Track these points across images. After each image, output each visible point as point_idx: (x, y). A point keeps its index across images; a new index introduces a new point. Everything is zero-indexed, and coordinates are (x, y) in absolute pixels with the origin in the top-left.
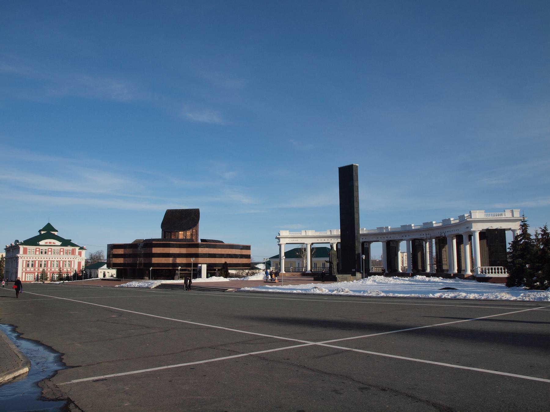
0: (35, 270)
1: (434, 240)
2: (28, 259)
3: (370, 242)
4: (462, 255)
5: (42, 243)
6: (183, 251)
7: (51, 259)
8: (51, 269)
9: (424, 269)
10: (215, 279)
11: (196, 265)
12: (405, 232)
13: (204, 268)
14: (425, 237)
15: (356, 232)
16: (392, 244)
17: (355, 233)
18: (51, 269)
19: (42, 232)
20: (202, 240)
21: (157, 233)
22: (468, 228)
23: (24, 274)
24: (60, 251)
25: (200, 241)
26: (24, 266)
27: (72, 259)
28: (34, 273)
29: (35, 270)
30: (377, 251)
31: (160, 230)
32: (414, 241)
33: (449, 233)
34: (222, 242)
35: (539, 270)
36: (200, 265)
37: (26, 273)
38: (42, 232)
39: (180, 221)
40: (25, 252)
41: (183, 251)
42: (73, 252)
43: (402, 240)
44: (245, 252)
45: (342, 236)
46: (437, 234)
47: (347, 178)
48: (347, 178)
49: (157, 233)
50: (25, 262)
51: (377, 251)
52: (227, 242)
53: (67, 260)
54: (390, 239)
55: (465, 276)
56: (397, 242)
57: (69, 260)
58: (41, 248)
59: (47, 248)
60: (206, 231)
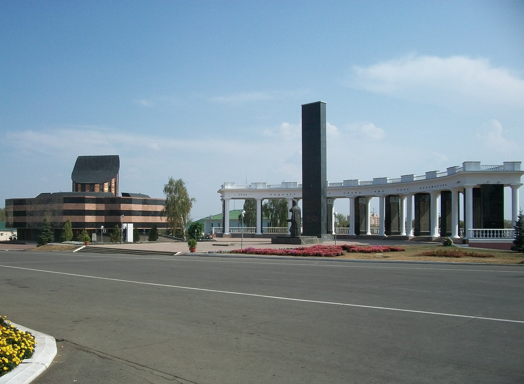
1: (413, 197)
3: (333, 198)
9: (329, 232)
10: (145, 246)
12: (379, 185)
13: (130, 228)
14: (403, 192)
15: (322, 185)
16: (361, 201)
17: (320, 186)
20: (124, 194)
22: (459, 182)
25: (120, 195)
30: (342, 208)
32: (388, 197)
33: (434, 189)
34: (148, 196)
35: (415, 234)
36: (125, 225)
43: (374, 196)
46: (418, 190)
47: (312, 117)
48: (312, 117)
51: (342, 208)
54: (360, 195)
55: (433, 240)
56: (367, 198)
60: (127, 182)
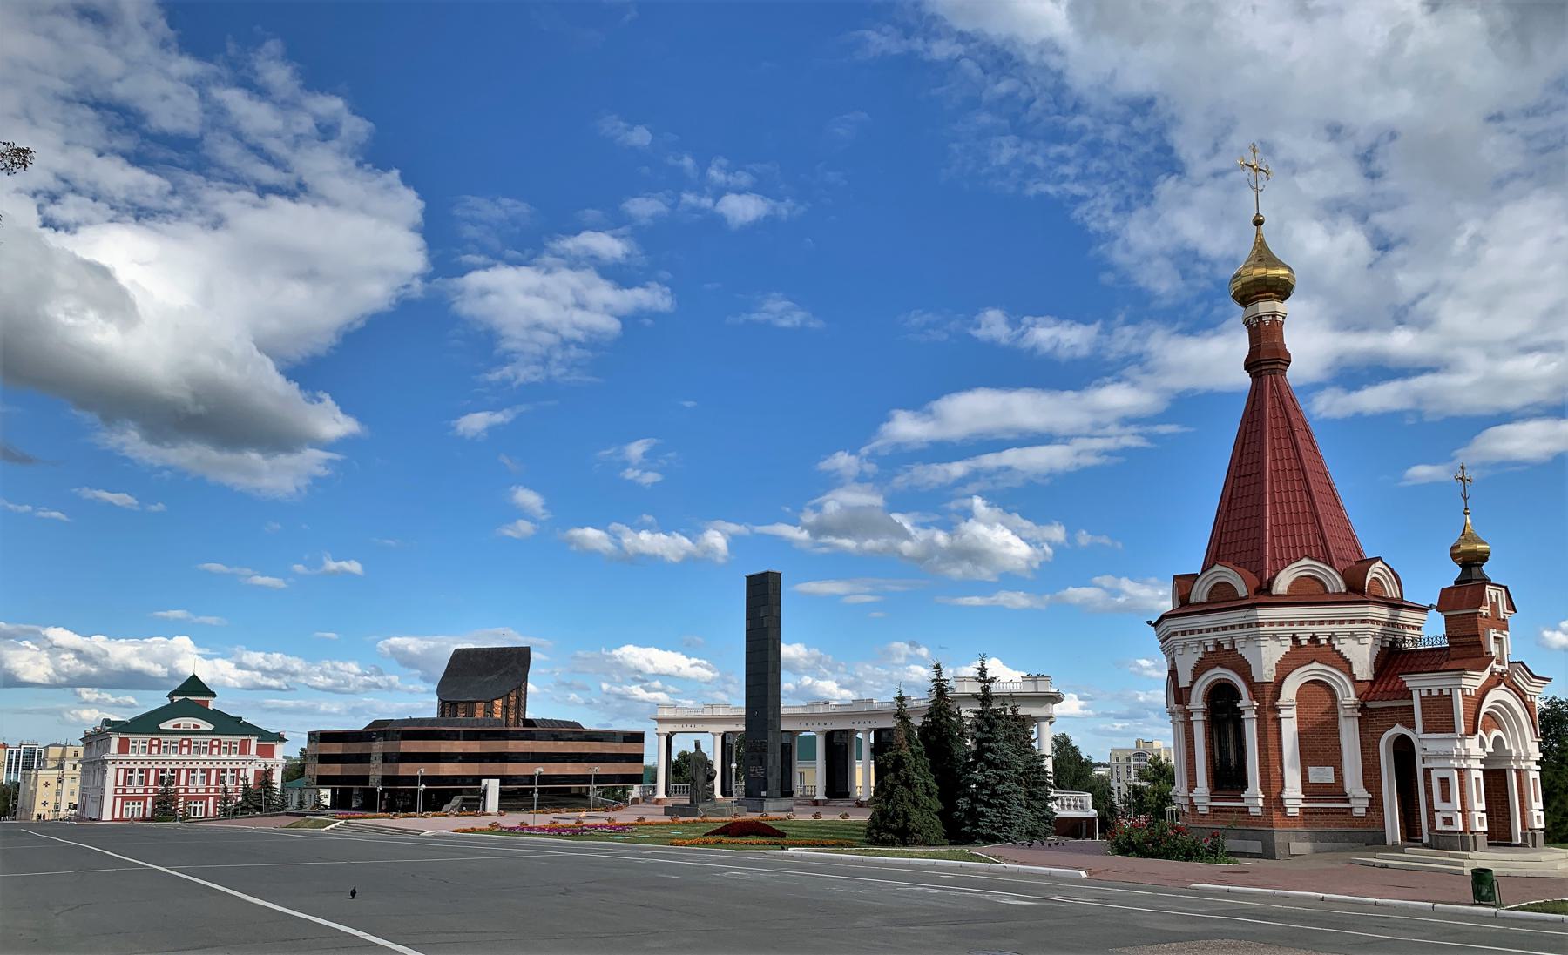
0: (146, 791)
2: (132, 765)
4: (1273, 758)
5: (168, 725)
6: (474, 747)
7: (188, 765)
8: (186, 790)
11: (477, 779)
13: (493, 787)
18: (186, 790)
19: (176, 699)
21: (423, 704)
23: (119, 801)
24: (151, 745)
26: (120, 783)
27: (241, 765)
28: (145, 799)
29: (146, 791)
31: (435, 699)
34: (577, 725)
37: (123, 799)
38: (176, 699)
39: (487, 675)
40: (124, 747)
41: (474, 747)
42: (244, 748)
44: (630, 748)
45: (749, 719)
47: (763, 595)
48: (763, 595)
49: (423, 704)
50: (121, 772)
52: (589, 724)
53: (227, 765)
57: (234, 766)
58: (163, 738)
59: (178, 738)
